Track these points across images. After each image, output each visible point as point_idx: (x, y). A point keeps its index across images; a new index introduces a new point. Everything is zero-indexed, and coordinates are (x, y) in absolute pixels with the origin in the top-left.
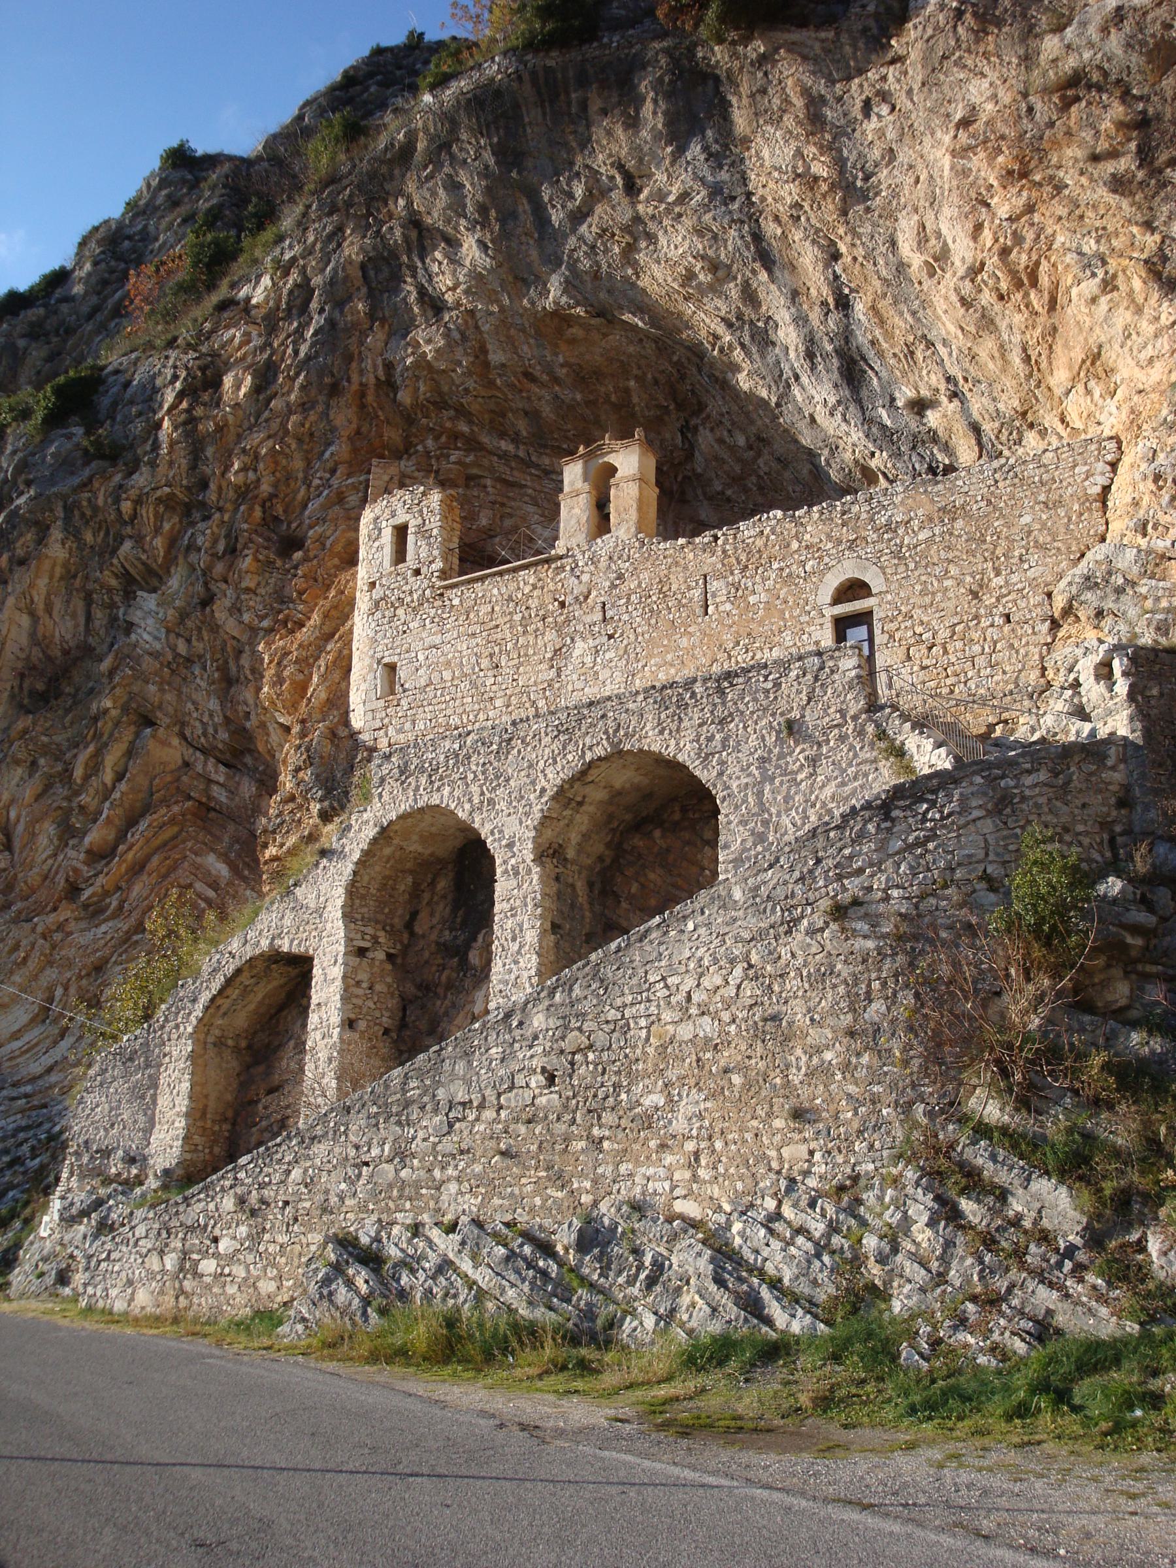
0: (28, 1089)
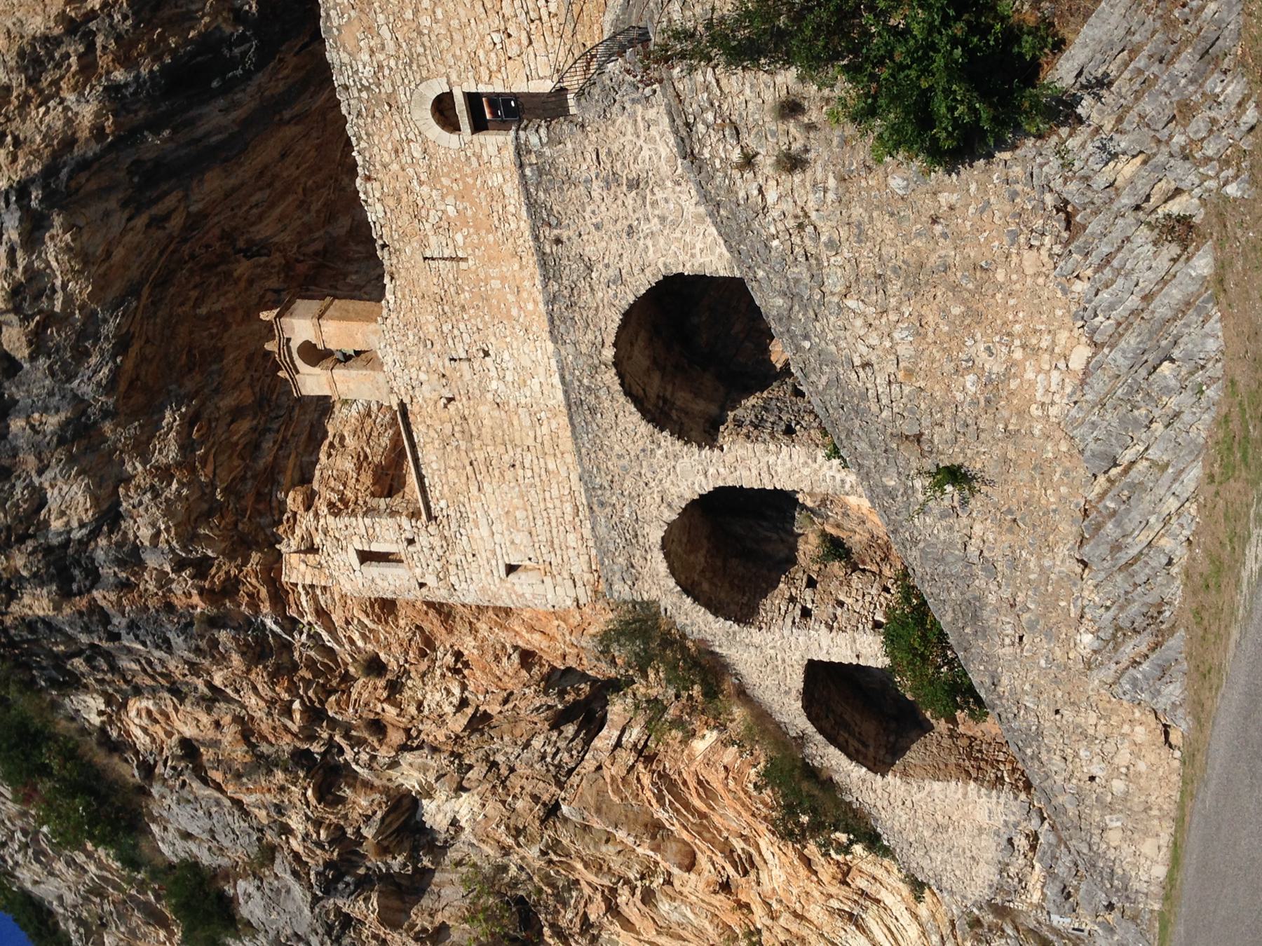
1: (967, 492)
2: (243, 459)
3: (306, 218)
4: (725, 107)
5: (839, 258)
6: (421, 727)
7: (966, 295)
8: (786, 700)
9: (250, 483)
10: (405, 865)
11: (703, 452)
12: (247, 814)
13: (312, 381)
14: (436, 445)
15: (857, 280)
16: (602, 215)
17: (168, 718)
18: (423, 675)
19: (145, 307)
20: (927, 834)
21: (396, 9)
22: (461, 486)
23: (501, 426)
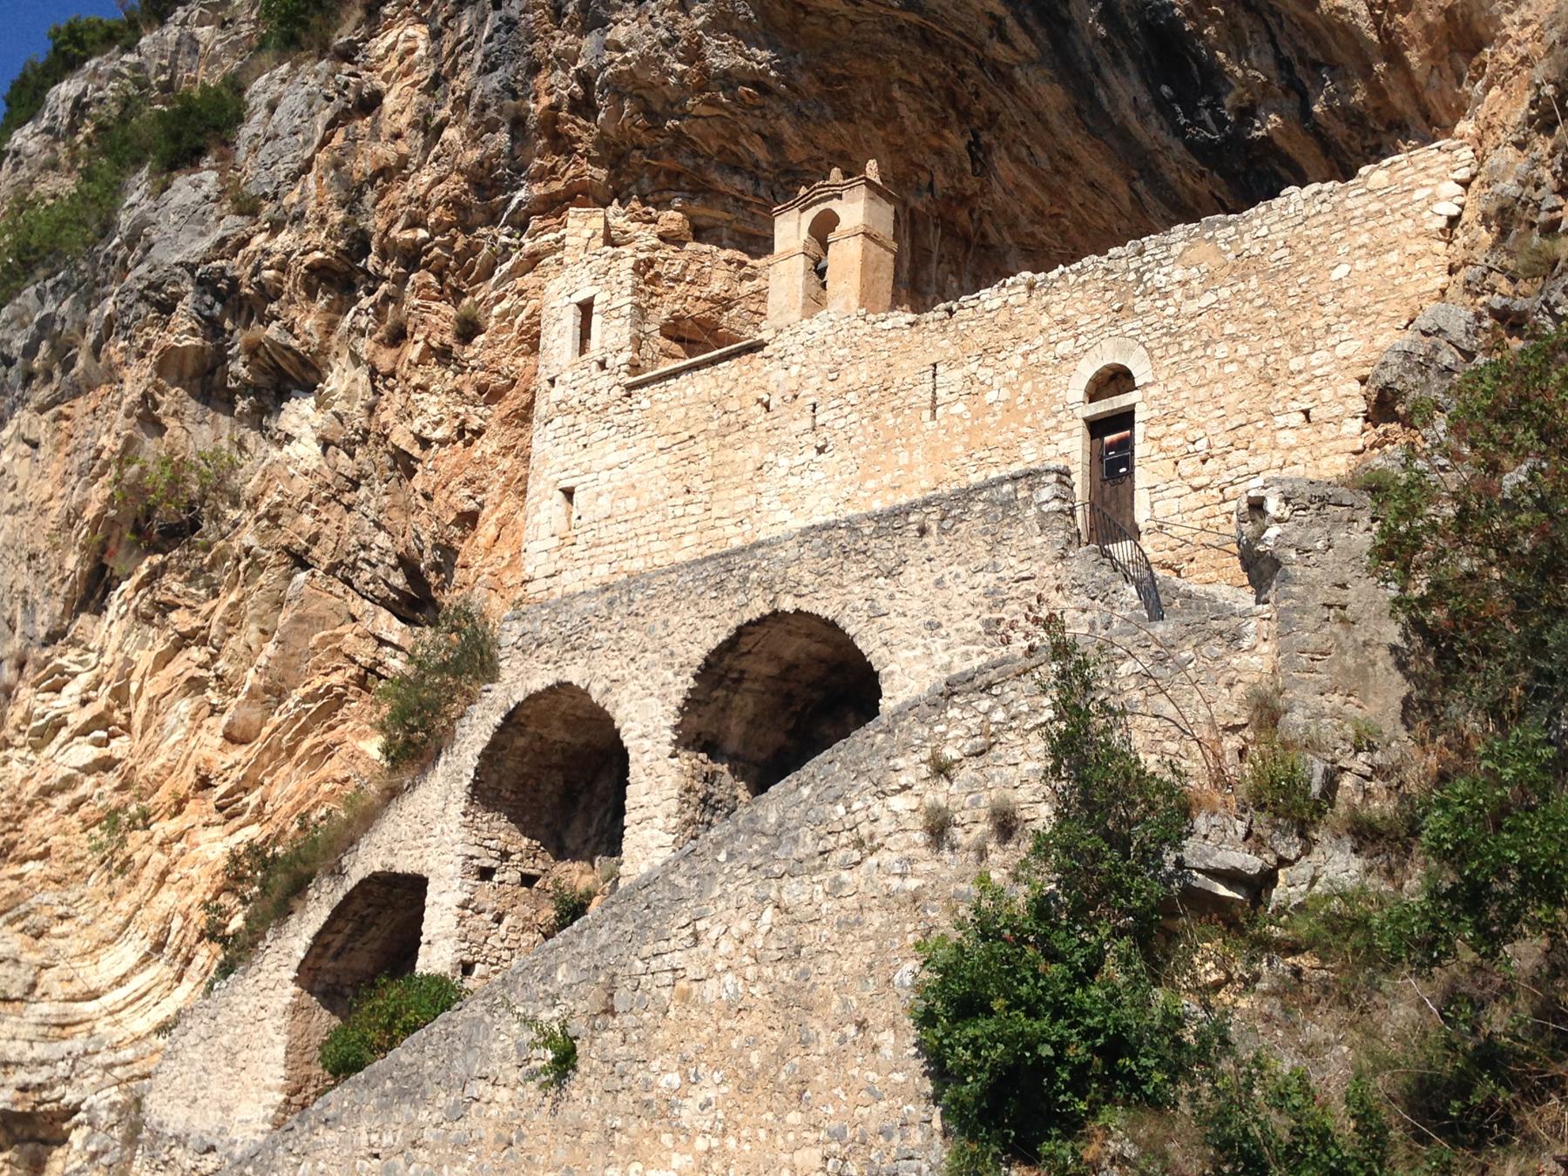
0: (128, 1053)
1: (544, 1078)
2: (719, 153)
3: (1023, 220)
4: (1011, 736)
5: (821, 896)
6: (397, 390)
7: (772, 1072)
8: (382, 851)
9: (690, 163)
10: (237, 379)
11: (668, 732)
12: (295, 179)
13: (791, 229)
14: (714, 392)
15: (794, 922)
16: (953, 588)
17: (406, 74)
18: (459, 392)
19: (895, 18)
20: (225, 1040)
21: (1235, 313)
22: (667, 426)
23: (735, 473)
